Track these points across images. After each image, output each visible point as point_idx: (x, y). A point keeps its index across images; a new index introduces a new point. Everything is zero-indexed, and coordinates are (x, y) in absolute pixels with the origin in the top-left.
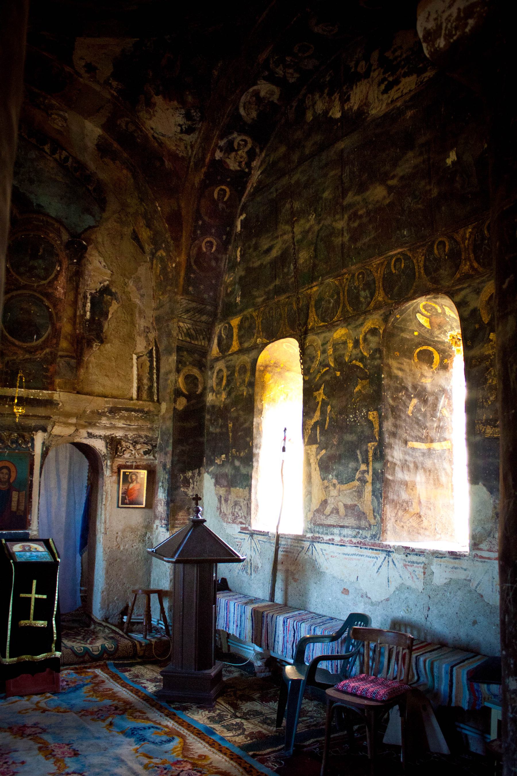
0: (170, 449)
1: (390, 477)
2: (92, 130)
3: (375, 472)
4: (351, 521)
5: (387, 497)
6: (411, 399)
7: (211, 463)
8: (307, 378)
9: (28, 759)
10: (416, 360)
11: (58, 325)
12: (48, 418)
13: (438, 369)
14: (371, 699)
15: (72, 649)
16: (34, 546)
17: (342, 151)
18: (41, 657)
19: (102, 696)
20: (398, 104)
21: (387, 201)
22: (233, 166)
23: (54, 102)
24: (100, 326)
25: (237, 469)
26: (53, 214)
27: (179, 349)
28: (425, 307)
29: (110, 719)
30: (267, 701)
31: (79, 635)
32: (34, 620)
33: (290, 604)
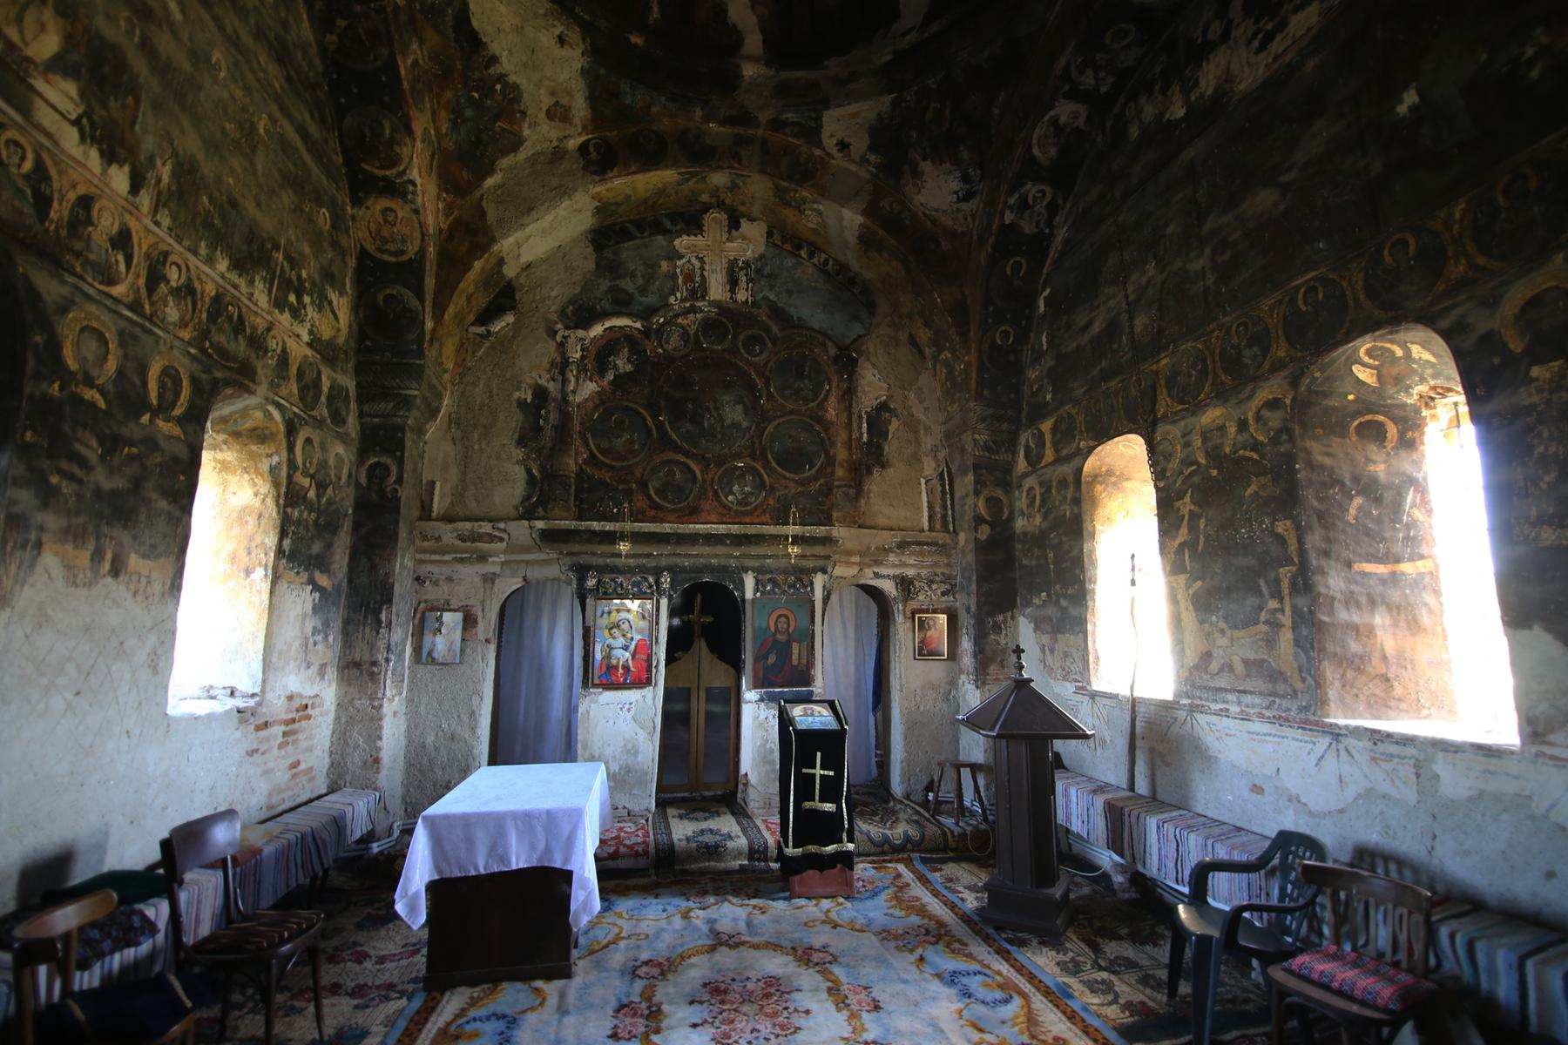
0: (974, 587)
1: (1325, 618)
2: (851, 219)
3: (1296, 611)
4: (1260, 684)
5: (1322, 650)
6: (1351, 498)
7: (1028, 603)
8: (1161, 484)
9: (813, 1007)
10: (1354, 438)
11: (832, 452)
12: (828, 557)
13: (1396, 448)
14: (1362, 1003)
15: (868, 834)
16: (817, 708)
18: (830, 849)
19: (908, 908)
20: (1288, 58)
21: (1282, 207)
22: (1028, 228)
23: (805, 194)
24: (880, 448)
25: (1064, 610)
26: (816, 327)
27: (976, 467)
28: (1369, 353)
29: (920, 951)
30: (1143, 944)
31: (875, 814)
32: (821, 801)
33: (1160, 797)
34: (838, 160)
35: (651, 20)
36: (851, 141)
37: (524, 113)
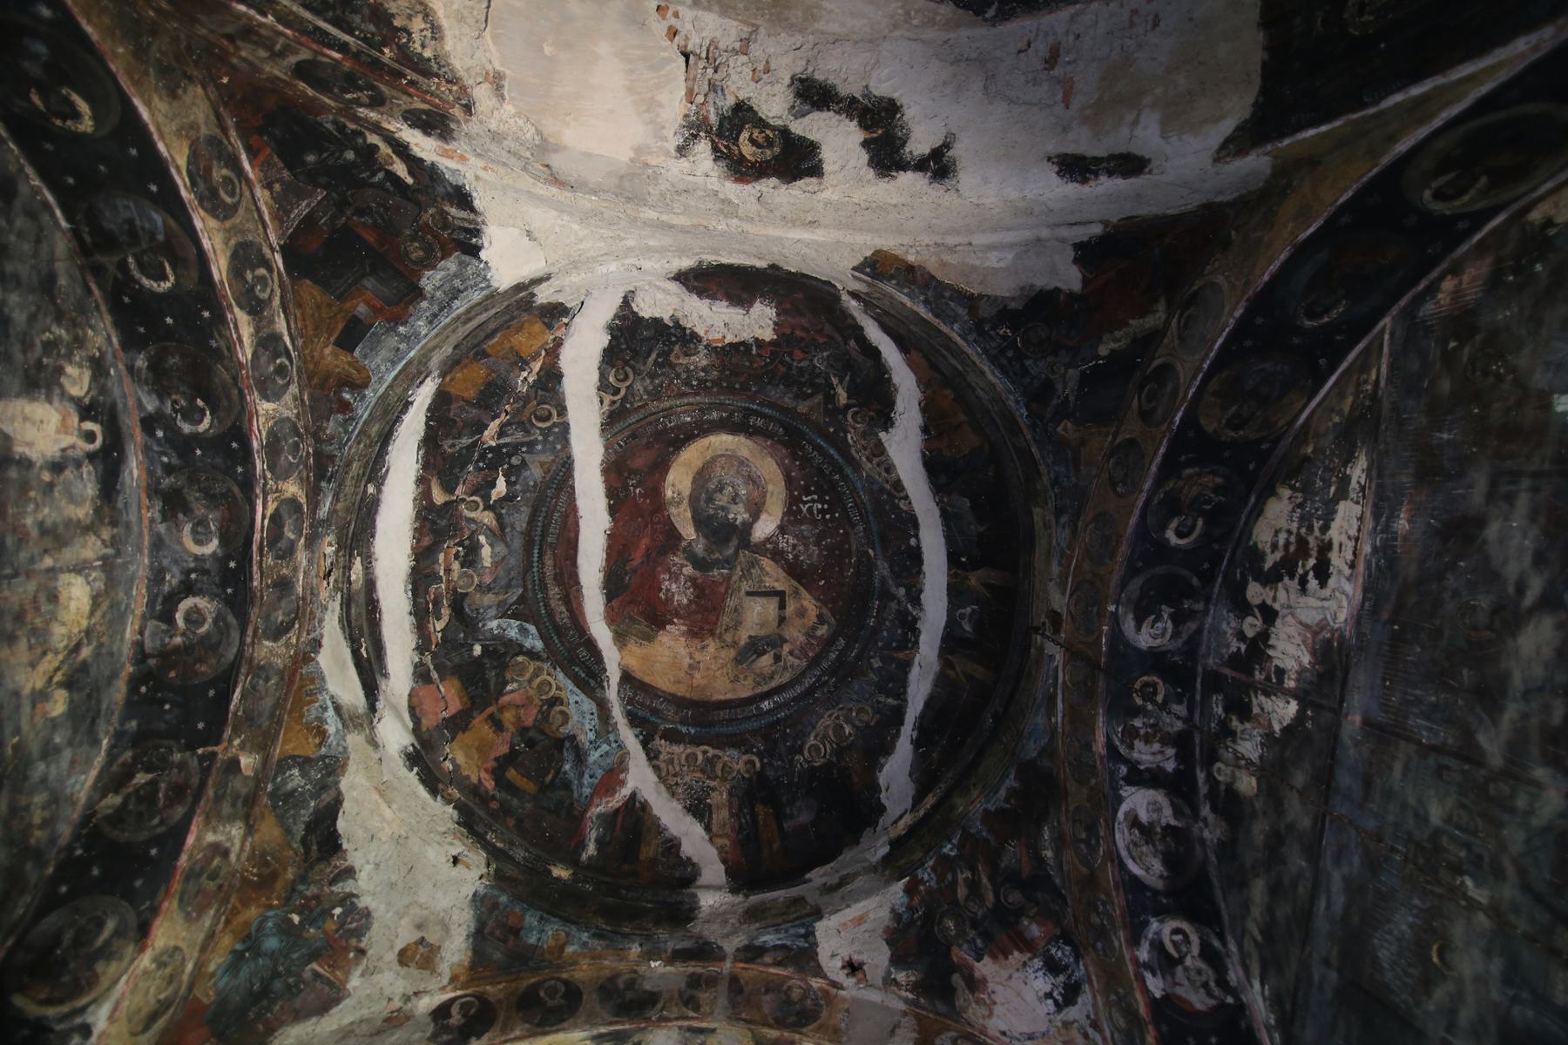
17: (1367, 722)
34: (851, 988)
35: (584, 857)
36: (864, 958)
37: (362, 952)
